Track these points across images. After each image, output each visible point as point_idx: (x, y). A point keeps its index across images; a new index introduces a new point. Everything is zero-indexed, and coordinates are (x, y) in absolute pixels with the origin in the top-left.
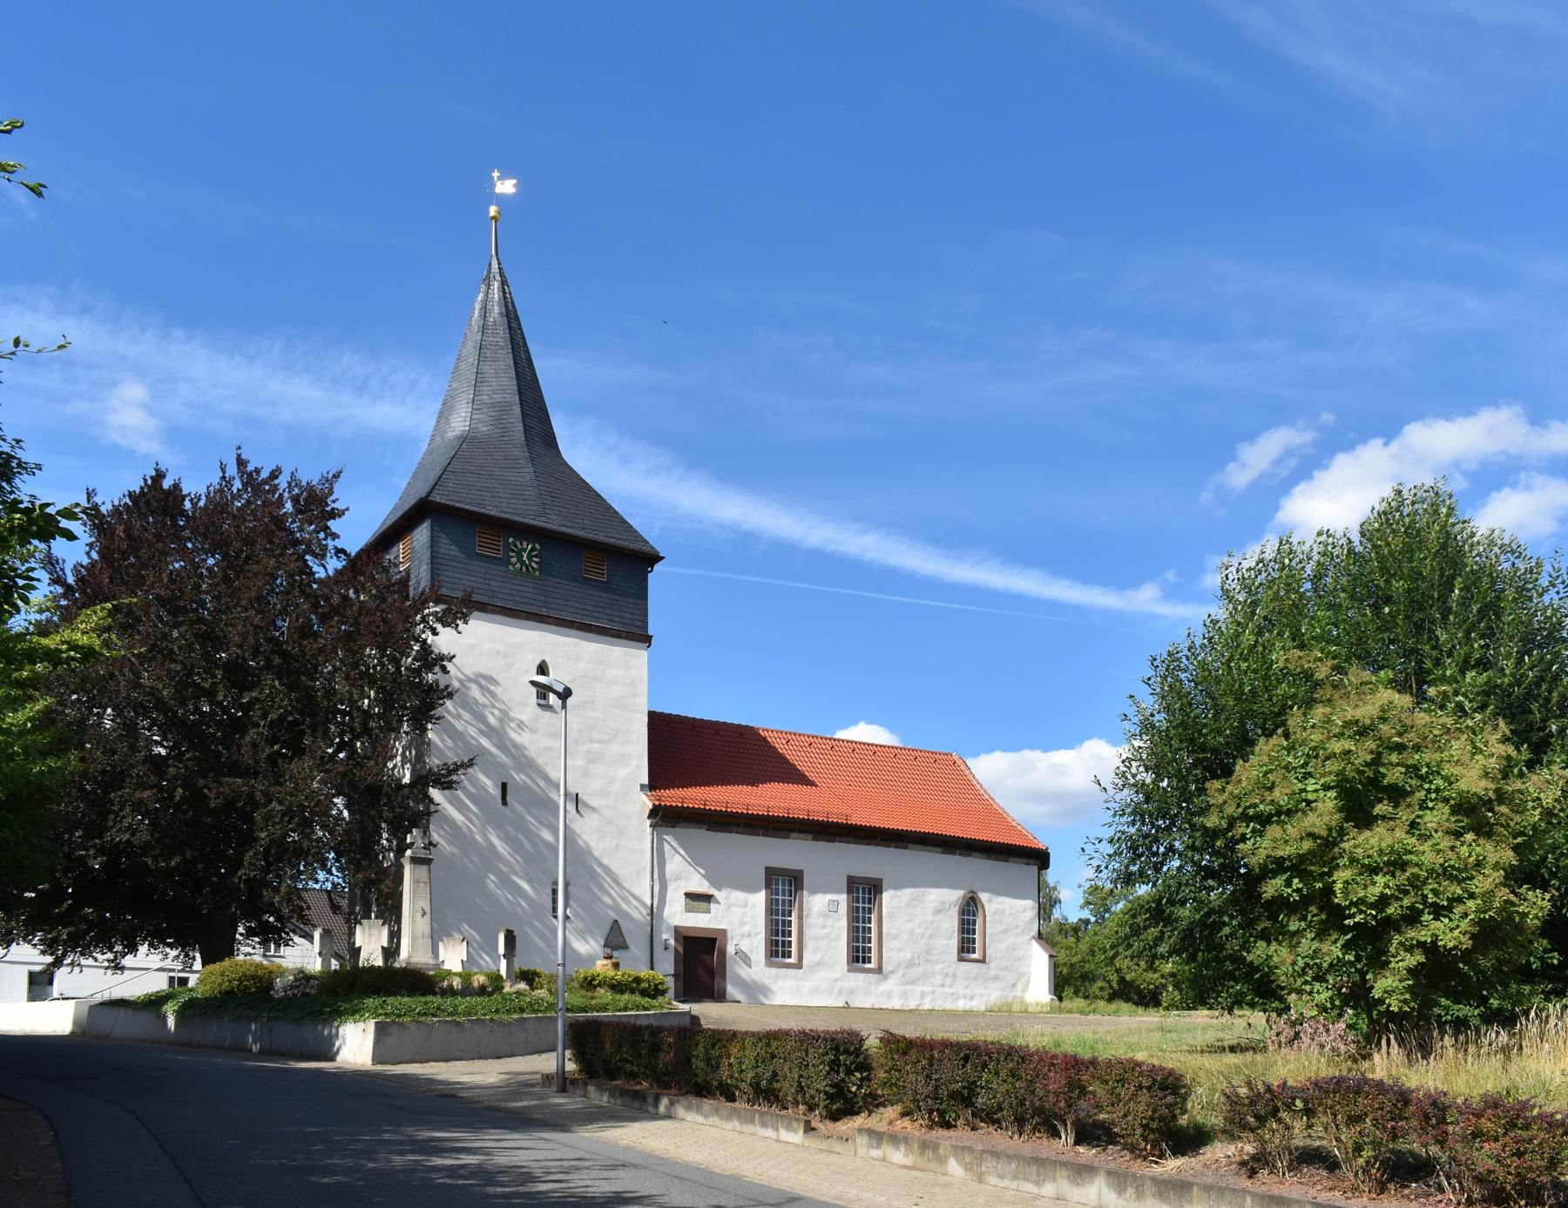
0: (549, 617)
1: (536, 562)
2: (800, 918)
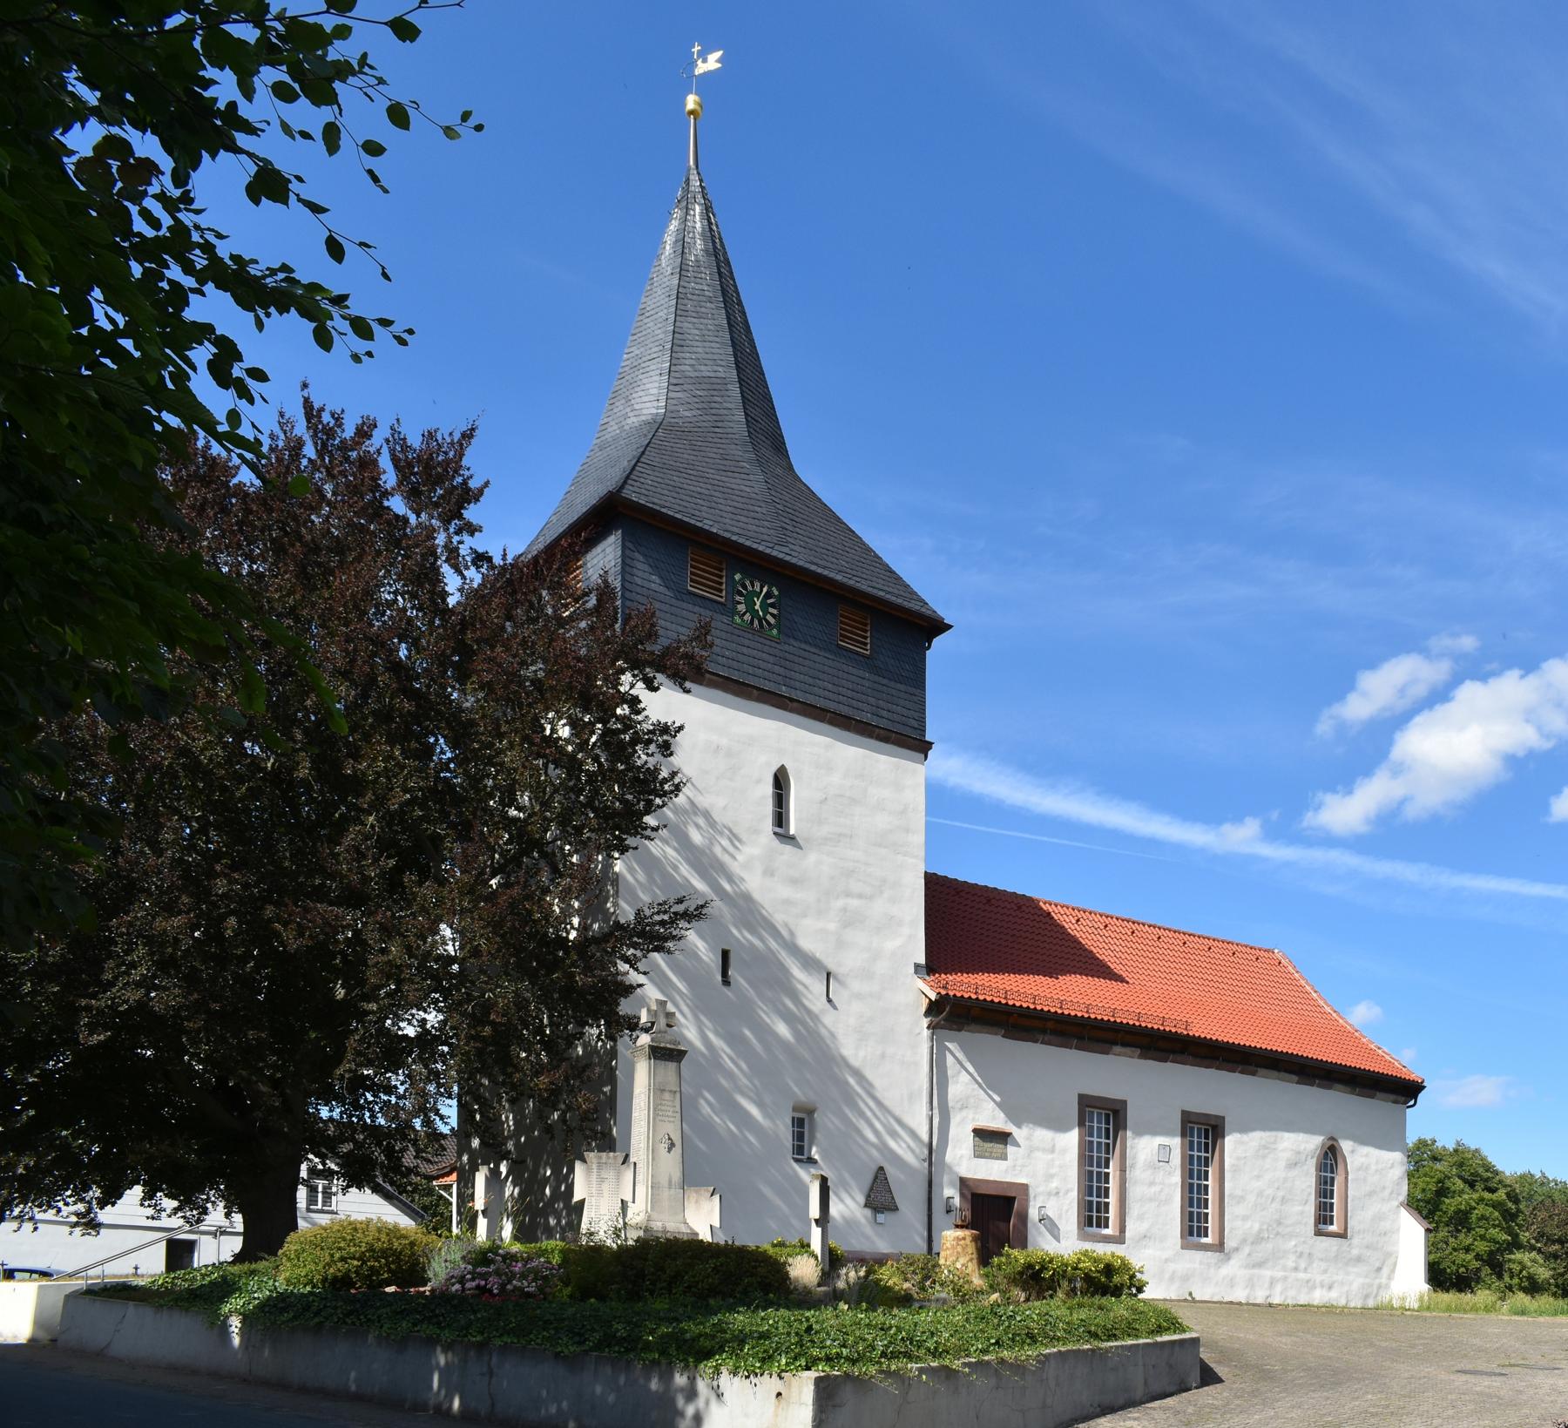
0: (792, 700)
1: (772, 615)
2: (1123, 1170)
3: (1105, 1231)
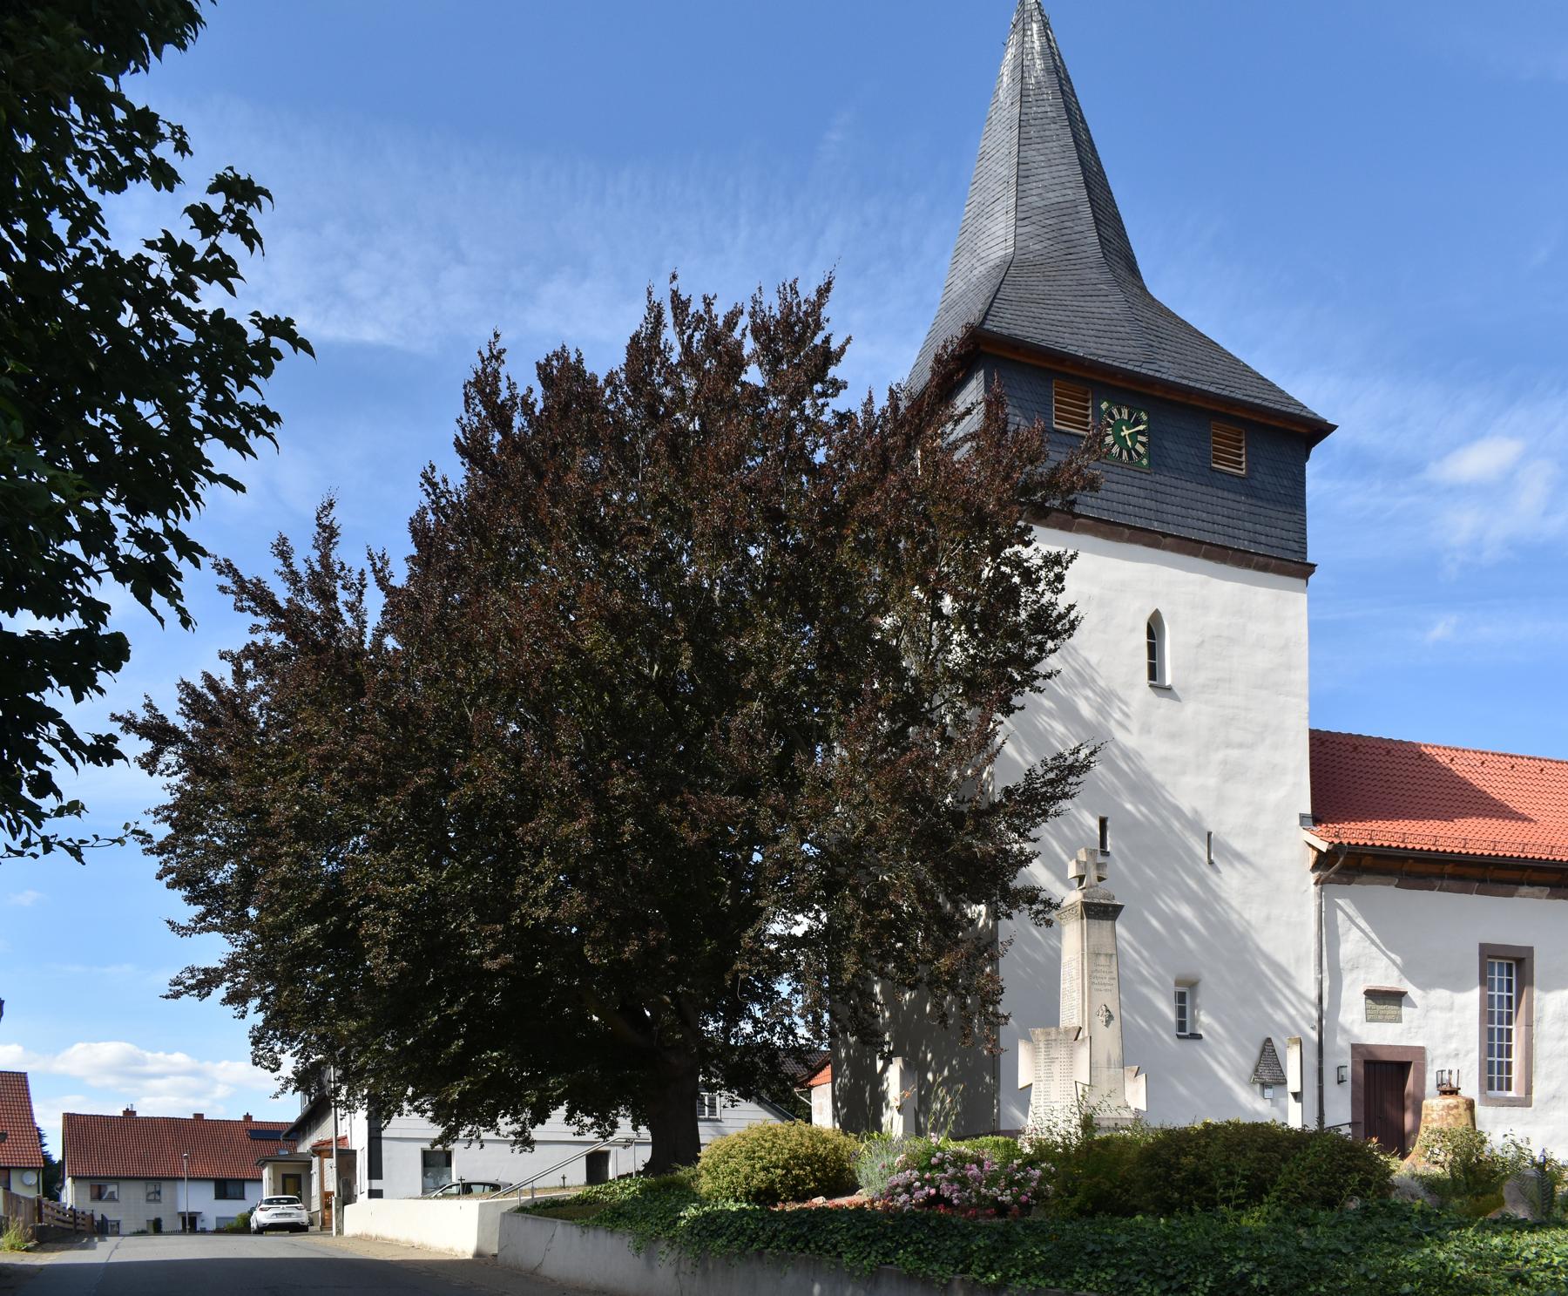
0: (1165, 535)
1: (1142, 443)
2: (1529, 1025)
3: (1511, 1094)
